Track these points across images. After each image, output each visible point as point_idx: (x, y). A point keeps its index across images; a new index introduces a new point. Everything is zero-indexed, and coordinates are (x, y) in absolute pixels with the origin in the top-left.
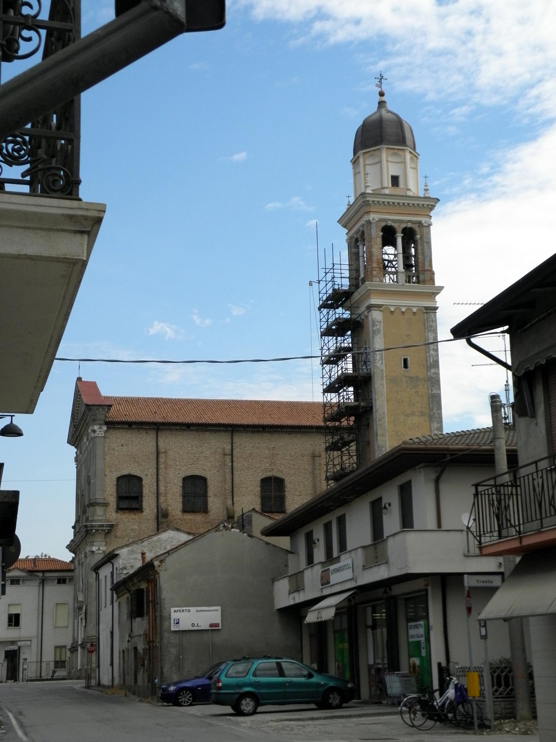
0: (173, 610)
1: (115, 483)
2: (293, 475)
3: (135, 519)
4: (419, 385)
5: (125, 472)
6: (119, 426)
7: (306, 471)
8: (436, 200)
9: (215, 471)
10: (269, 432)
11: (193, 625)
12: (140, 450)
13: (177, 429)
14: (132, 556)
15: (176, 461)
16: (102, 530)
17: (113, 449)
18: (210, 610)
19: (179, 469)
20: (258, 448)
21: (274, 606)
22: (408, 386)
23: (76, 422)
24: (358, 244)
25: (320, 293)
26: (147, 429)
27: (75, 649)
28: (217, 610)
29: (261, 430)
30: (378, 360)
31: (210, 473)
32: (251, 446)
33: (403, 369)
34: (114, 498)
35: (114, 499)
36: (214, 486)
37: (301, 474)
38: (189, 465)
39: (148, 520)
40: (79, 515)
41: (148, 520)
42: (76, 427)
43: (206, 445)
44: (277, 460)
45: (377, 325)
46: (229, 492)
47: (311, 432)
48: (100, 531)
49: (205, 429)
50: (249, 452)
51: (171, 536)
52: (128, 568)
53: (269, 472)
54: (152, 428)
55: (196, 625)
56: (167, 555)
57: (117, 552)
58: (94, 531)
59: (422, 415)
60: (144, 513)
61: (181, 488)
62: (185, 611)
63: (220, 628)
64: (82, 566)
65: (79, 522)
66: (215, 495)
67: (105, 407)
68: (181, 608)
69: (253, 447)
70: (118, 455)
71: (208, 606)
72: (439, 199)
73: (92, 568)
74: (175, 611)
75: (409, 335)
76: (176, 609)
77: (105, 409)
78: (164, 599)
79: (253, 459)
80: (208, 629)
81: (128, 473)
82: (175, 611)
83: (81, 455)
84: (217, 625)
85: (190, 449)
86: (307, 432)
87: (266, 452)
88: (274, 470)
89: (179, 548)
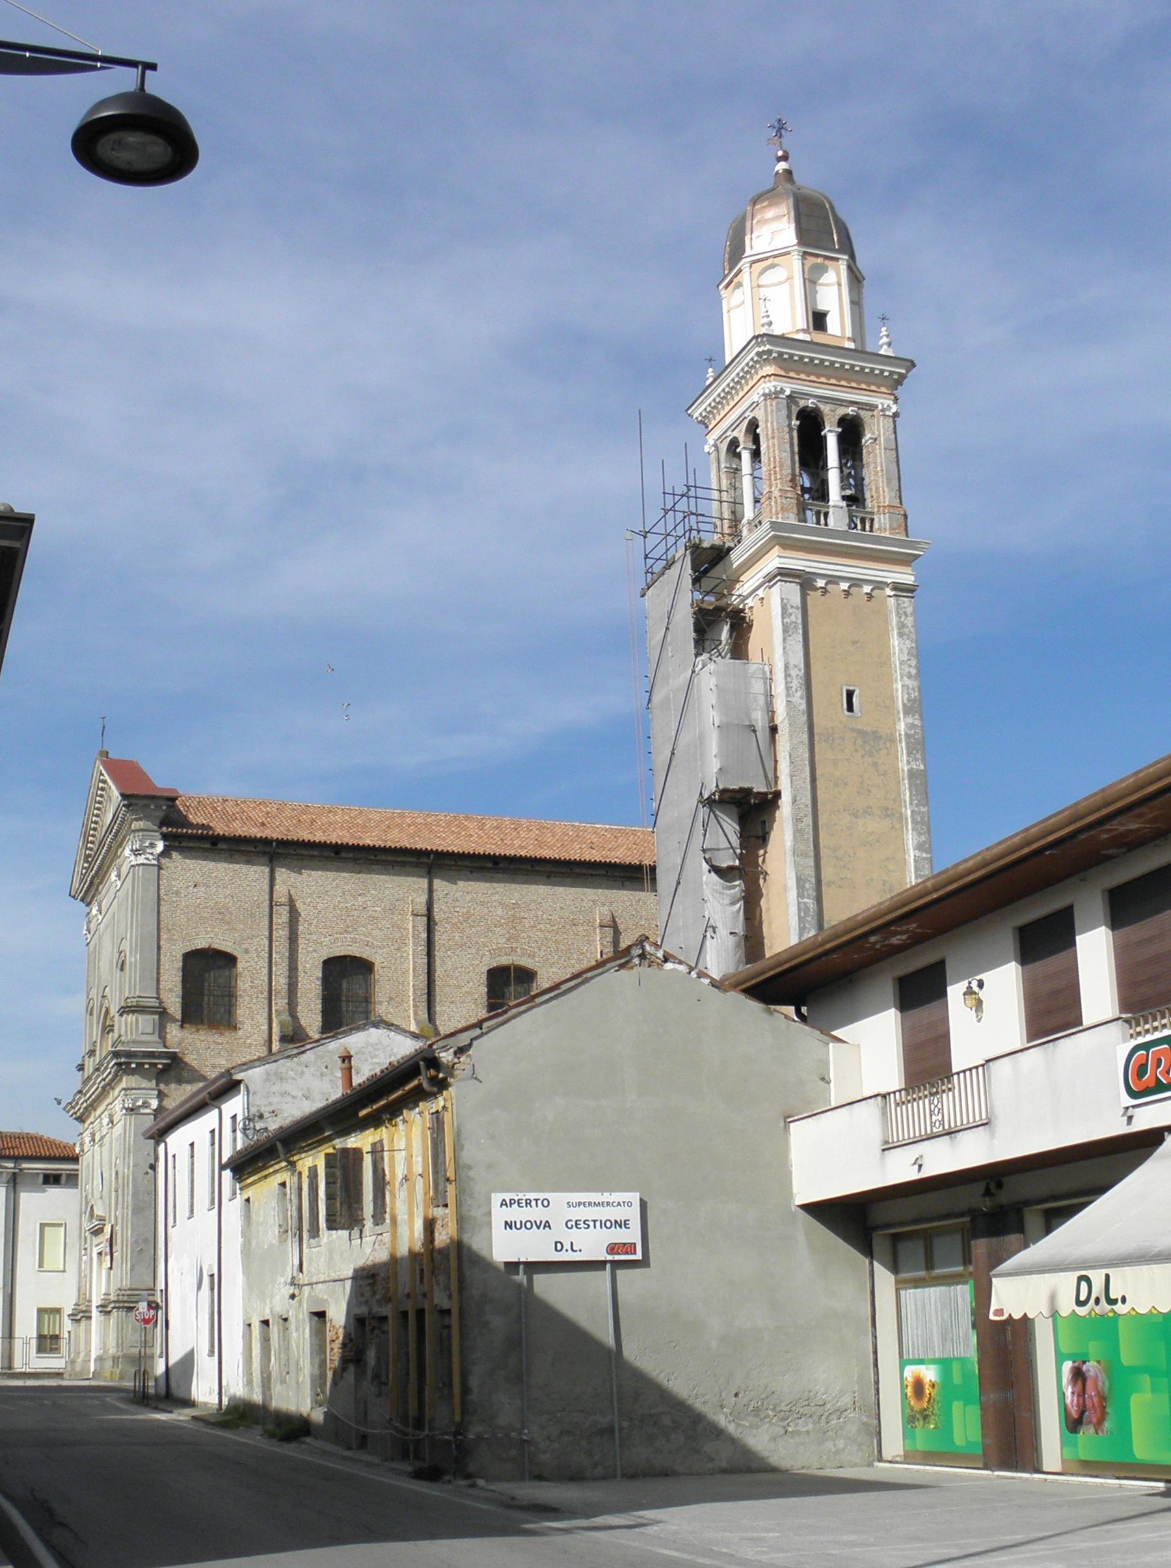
0: (497, 1198)
1: (180, 964)
2: (554, 963)
3: (222, 1044)
4: (880, 750)
5: (201, 944)
6: (191, 845)
7: (581, 957)
8: (909, 364)
9: (393, 947)
10: (505, 871)
11: (559, 1246)
12: (233, 897)
13: (313, 856)
14: (275, 1088)
15: (310, 924)
16: (150, 1064)
17: (177, 893)
18: (608, 1203)
19: (316, 942)
20: (482, 903)
21: (790, 1195)
22: (856, 750)
23: (91, 849)
24: (738, 450)
25: (646, 557)
26: (249, 852)
27: (86, 1314)
28: (630, 1204)
29: (490, 865)
30: (793, 689)
31: (380, 951)
32: (468, 898)
33: (846, 713)
34: (177, 996)
35: (178, 1000)
36: (389, 980)
37: (572, 962)
38: (337, 933)
39: (249, 1047)
40: (94, 1040)
41: (249, 1047)
42: (90, 859)
43: (373, 892)
44: (523, 932)
45: (791, 614)
46: (422, 994)
47: (592, 875)
48: (147, 1066)
49: (373, 857)
50: (465, 910)
51: (373, 1040)
52: (266, 1115)
53: (506, 955)
54: (259, 852)
55: (567, 1246)
56: (477, 1032)
57: (238, 1077)
58: (133, 1066)
59: (887, 816)
60: (240, 1033)
61: (319, 983)
62: (533, 1203)
63: (638, 1256)
64: (101, 1146)
65: (95, 1055)
66: (391, 999)
67: (161, 802)
68: (521, 1196)
69: (472, 900)
70: (187, 907)
71: (602, 1190)
72: (916, 362)
73: (147, 1131)
74: (503, 1203)
75: (857, 642)
76: (508, 1196)
77: (161, 807)
78: (470, 1167)
79: (471, 927)
80: (603, 1259)
81: (207, 946)
82: (503, 1203)
83: (100, 917)
84: (629, 1248)
85: (339, 899)
86: (584, 875)
87: (500, 912)
88: (516, 951)
89: (564, 987)
